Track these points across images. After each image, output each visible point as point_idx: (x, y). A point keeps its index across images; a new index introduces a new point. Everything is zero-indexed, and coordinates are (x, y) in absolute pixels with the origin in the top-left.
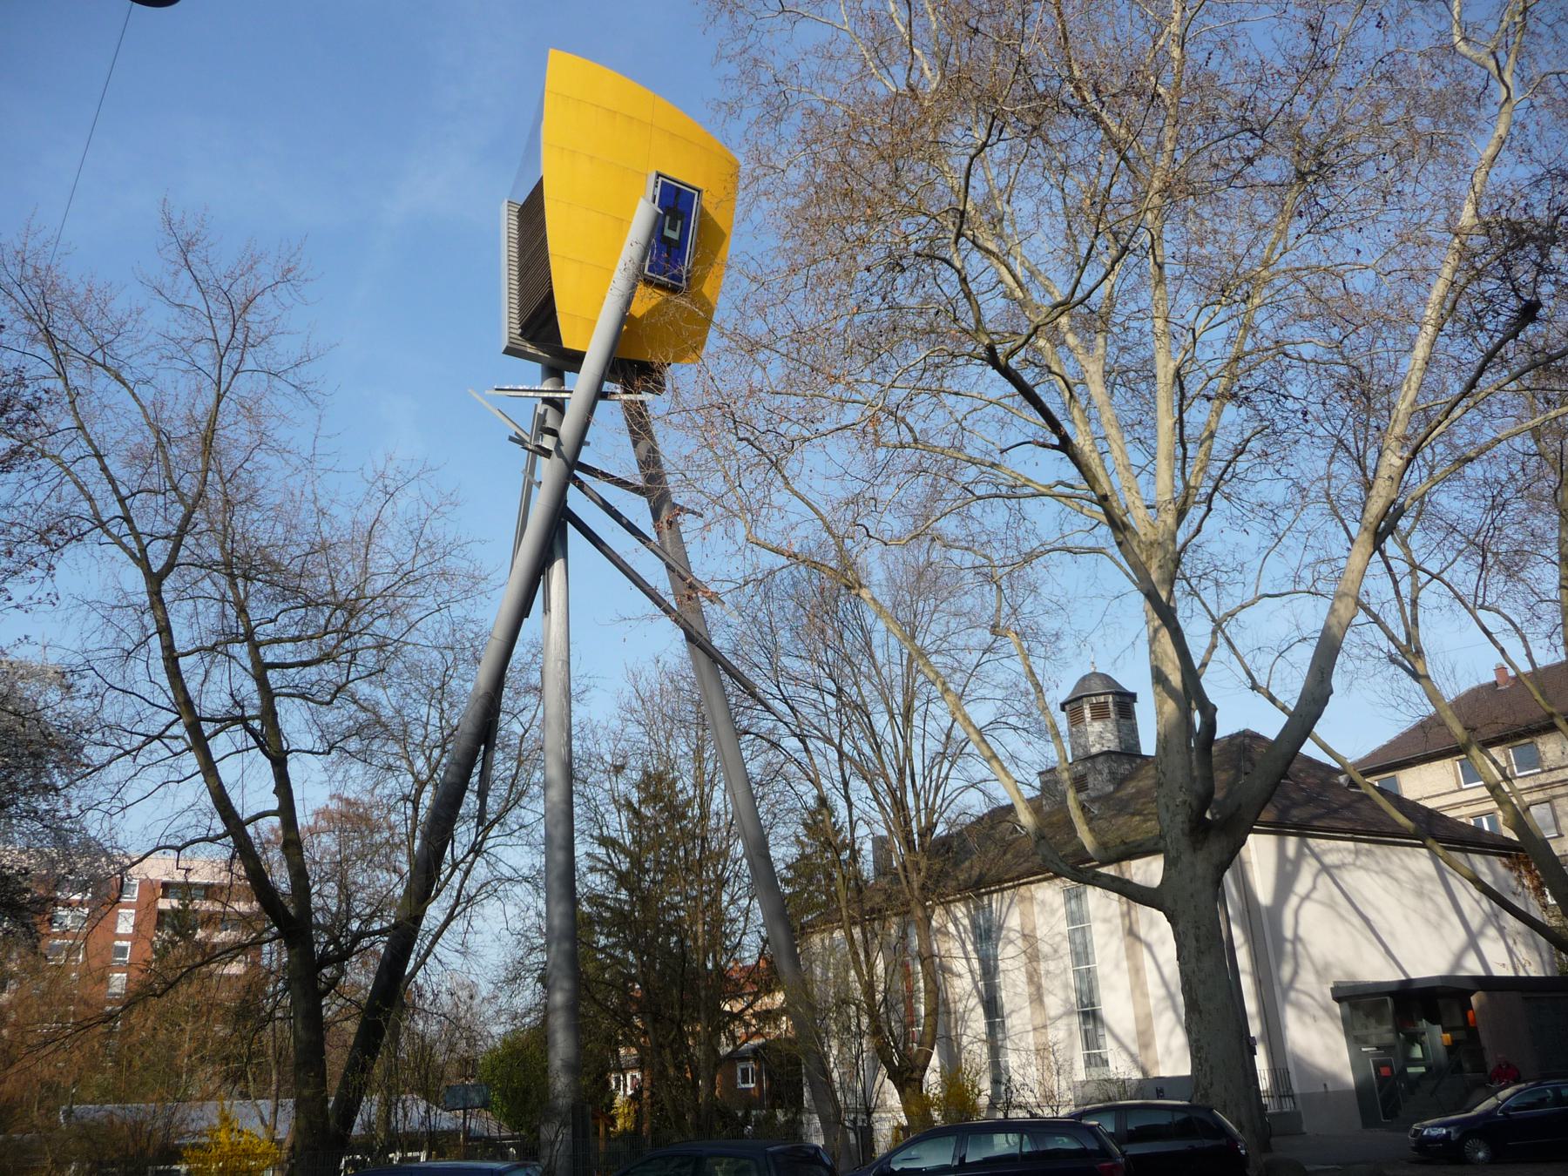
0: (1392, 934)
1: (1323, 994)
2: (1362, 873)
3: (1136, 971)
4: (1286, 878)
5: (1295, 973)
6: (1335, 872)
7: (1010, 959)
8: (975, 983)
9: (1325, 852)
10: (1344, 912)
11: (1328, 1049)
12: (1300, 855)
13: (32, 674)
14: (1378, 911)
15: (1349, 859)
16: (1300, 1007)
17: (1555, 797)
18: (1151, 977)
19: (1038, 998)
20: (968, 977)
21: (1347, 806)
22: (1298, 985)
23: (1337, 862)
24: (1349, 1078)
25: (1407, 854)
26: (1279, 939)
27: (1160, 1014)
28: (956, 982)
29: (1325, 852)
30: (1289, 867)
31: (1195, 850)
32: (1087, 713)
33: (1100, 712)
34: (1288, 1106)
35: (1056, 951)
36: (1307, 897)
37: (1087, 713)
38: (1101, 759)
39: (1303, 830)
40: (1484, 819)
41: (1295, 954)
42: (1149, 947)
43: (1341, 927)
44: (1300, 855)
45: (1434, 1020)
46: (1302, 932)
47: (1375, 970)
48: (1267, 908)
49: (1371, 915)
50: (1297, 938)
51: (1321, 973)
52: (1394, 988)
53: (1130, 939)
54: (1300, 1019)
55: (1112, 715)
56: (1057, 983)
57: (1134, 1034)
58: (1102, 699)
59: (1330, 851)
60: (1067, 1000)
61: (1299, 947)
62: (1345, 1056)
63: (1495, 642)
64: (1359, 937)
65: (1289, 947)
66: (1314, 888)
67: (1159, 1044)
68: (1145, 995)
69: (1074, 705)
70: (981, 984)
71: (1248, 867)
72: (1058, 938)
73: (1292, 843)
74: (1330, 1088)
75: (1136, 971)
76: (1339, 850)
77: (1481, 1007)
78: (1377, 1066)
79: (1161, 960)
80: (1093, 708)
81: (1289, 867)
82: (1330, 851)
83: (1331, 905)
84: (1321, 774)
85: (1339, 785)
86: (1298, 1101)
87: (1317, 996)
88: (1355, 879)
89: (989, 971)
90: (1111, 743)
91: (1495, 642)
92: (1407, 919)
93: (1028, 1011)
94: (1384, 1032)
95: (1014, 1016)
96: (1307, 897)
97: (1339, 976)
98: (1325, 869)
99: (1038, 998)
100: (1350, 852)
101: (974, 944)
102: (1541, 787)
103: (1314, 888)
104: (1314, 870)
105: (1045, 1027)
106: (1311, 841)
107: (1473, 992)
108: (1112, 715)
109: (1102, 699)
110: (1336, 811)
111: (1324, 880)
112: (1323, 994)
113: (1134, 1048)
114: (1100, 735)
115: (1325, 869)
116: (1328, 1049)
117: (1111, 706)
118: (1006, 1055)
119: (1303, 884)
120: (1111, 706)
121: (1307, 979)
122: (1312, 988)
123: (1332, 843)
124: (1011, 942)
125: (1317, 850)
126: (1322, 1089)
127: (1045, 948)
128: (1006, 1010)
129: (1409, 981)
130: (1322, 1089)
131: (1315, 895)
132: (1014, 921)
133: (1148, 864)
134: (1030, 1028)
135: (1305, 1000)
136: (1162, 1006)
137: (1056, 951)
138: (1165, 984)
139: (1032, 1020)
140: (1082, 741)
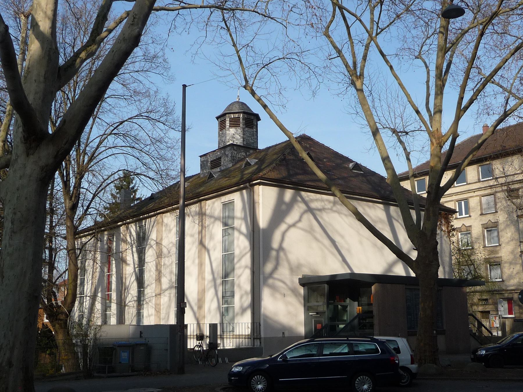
0: (349, 251)
1: (292, 282)
2: (336, 215)
3: (201, 265)
4: (280, 213)
5: (276, 268)
6: (317, 213)
7: (150, 255)
8: (135, 268)
9: (312, 201)
10: (318, 236)
11: (289, 313)
12: (294, 200)
13: (346, 215)
14: (342, 237)
15: (329, 206)
16: (274, 288)
17: (496, 192)
18: (208, 269)
19: (159, 280)
20: (132, 266)
21: (344, 178)
22: (276, 276)
23: (320, 207)
24: (301, 330)
25: (369, 207)
26: (268, 248)
27: (209, 289)
28: (128, 268)
29: (312, 201)
30: (284, 207)
31: (28, 155)
32: (228, 123)
33: (235, 123)
34: (257, 343)
35: (169, 252)
36: (294, 225)
37: (228, 123)
38: (228, 148)
39: (298, 186)
40: (463, 203)
41: (277, 259)
42: (208, 251)
43: (315, 244)
44: (294, 200)
45: (354, 298)
46: (285, 245)
47: (331, 267)
48: (263, 230)
49: (337, 239)
50: (281, 248)
51: (292, 270)
52: (327, 279)
53: (201, 246)
54: (273, 295)
55: (241, 125)
56: (168, 270)
57: (196, 301)
58: (237, 116)
59: (317, 200)
60: (170, 280)
61: (282, 254)
62: (301, 316)
63: (387, 62)
64: (326, 251)
65: (274, 253)
66: (300, 220)
67: (206, 306)
68: (203, 279)
69: (222, 119)
70: (137, 269)
71: (256, 205)
72: (171, 245)
73: (289, 194)
74: (286, 335)
75: (201, 265)
76: (322, 200)
77: (376, 292)
78: (316, 322)
79: (213, 259)
80: (231, 120)
81: (284, 207)
82: (317, 200)
83: (310, 231)
84: (338, 161)
85: (347, 168)
86: (262, 340)
87: (288, 283)
88: (327, 218)
89: (142, 262)
90: (238, 140)
91: (387, 62)
92: (361, 243)
93: (154, 286)
94: (321, 304)
95: (149, 288)
96: (294, 225)
97: (306, 271)
98: (310, 210)
99: (159, 280)
100: (330, 202)
101: (136, 247)
102: (491, 187)
103: (300, 220)
104: (302, 210)
105: (160, 294)
106: (303, 193)
107: (373, 284)
108: (241, 125)
109: (237, 116)
110: (334, 179)
111: (308, 217)
112: (292, 282)
113: (195, 308)
114: (234, 135)
115: (310, 210)
116: (289, 313)
117: (241, 120)
118: (143, 309)
119: (291, 219)
120: (241, 120)
121: (283, 272)
122: (286, 277)
123: (318, 196)
124: (151, 246)
125: (307, 199)
126: (281, 335)
127: (165, 250)
128: (146, 285)
129: (353, 274)
130: (281, 335)
131: (300, 225)
132: (153, 236)
133: (214, 203)
134: (154, 295)
135: (279, 284)
136: (210, 285)
137: (169, 252)
138: (213, 273)
139: (155, 291)
140: (223, 139)
